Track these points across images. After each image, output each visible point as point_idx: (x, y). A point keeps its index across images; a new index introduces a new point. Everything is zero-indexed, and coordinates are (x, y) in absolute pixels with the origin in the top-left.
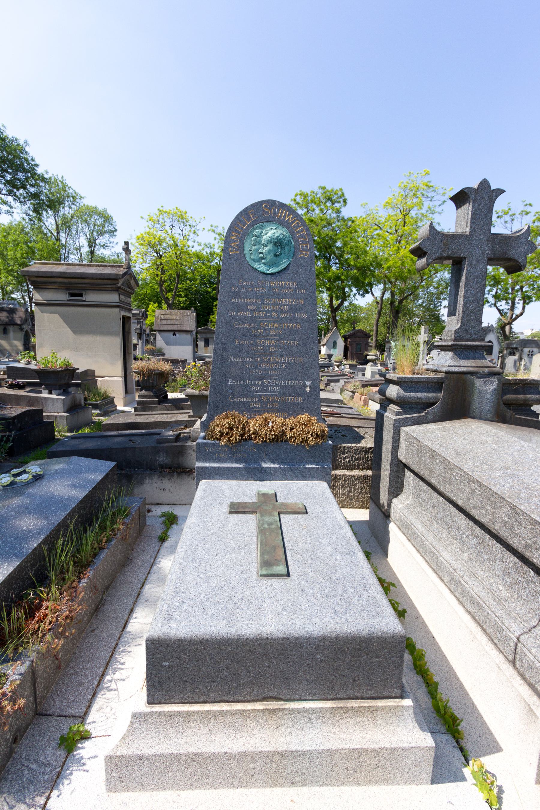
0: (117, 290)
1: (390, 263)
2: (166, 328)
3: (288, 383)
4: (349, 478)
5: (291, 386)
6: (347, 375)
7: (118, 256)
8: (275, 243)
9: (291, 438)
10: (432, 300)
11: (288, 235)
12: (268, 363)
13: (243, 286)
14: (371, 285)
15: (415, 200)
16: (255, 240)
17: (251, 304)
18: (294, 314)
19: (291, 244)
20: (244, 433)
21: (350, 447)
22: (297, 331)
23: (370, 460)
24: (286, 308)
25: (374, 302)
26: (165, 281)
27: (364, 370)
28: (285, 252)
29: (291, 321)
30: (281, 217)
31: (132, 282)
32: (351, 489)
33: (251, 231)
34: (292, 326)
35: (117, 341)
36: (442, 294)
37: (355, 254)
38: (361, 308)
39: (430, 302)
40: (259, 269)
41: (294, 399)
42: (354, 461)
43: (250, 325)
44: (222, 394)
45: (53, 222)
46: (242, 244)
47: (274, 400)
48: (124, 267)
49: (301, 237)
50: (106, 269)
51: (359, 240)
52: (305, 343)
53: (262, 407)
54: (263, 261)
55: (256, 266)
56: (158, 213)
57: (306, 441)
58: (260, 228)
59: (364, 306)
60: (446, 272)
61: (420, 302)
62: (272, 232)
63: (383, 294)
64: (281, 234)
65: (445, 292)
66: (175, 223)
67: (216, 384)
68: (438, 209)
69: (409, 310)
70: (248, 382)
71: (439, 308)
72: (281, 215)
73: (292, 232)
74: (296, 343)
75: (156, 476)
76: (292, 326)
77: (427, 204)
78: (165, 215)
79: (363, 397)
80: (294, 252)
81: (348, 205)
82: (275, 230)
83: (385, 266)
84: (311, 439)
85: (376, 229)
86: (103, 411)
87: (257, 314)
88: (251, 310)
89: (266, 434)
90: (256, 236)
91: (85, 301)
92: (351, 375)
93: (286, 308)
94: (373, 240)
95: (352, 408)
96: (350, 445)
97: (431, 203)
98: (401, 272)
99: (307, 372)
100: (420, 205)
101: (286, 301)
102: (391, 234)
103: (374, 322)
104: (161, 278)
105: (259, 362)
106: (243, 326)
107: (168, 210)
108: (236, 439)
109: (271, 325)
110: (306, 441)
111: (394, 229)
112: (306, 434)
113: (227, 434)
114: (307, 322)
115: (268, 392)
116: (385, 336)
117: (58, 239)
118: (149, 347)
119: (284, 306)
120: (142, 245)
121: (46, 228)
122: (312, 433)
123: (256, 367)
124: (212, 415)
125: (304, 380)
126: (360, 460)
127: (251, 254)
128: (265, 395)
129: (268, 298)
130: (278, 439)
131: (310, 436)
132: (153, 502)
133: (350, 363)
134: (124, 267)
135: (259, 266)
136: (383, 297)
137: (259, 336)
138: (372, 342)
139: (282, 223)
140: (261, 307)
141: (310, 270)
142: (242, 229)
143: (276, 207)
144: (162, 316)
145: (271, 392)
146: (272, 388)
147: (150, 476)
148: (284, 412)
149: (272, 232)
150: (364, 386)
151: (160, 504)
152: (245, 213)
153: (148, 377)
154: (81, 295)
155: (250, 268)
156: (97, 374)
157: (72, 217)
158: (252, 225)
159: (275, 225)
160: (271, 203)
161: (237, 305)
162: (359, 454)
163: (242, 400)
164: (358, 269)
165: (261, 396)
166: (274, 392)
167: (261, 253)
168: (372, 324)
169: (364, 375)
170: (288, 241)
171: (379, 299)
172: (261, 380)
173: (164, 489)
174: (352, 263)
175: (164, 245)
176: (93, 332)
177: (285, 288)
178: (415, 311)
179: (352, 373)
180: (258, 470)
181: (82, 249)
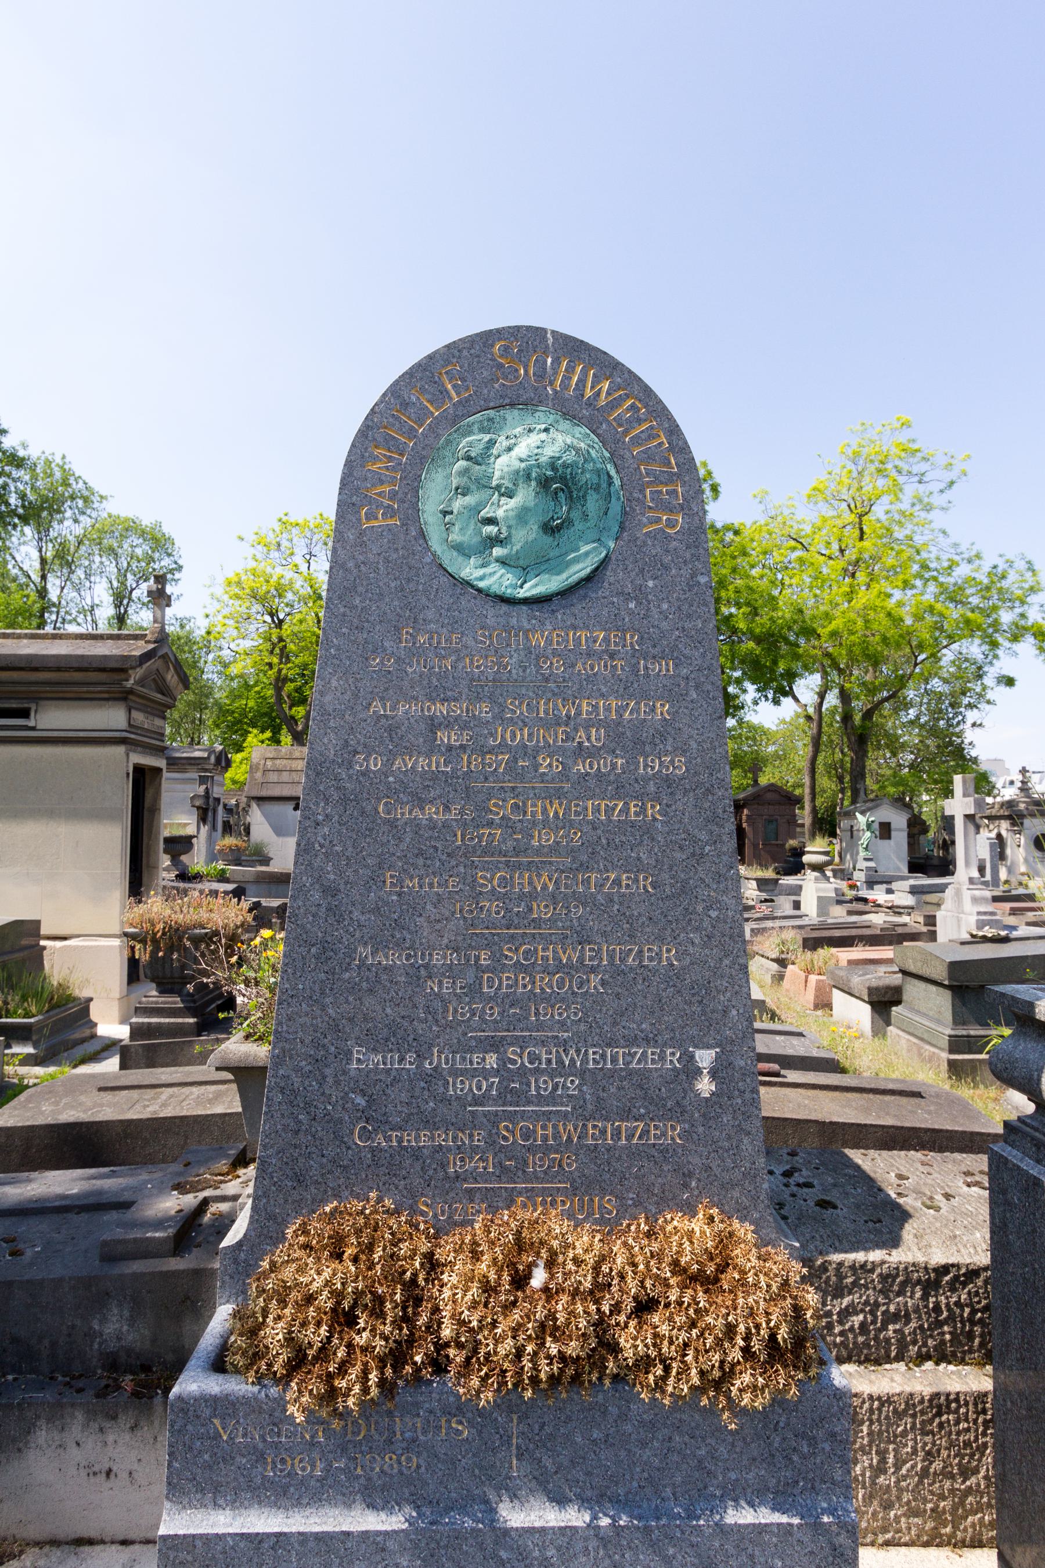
0: (125, 697)
1: (836, 624)
2: (276, 792)
3: (614, 1060)
4: (871, 1410)
5: (631, 1073)
6: (753, 907)
7: (182, 626)
8: (544, 483)
9: (644, 1363)
10: (941, 711)
11: (598, 452)
12: (525, 969)
13: (415, 652)
14: (791, 676)
15: (881, 482)
16: (466, 471)
17: (448, 723)
18: (632, 761)
19: (610, 483)
20: (411, 1341)
21: (863, 1266)
22: (647, 830)
23: (946, 1322)
24: (596, 737)
25: (798, 716)
26: (286, 680)
27: (797, 890)
28: (585, 516)
29: (620, 787)
30: (565, 386)
31: (171, 678)
32: (883, 1460)
33: (448, 442)
34: (626, 810)
35: (114, 837)
36: (964, 694)
37: (748, 604)
38: (765, 732)
39: (937, 713)
40: (481, 584)
41: (645, 1132)
42: (884, 1327)
43: (447, 809)
44: (320, 1113)
45: (35, 555)
46: (413, 487)
47: (556, 1136)
48: (148, 638)
49: (649, 457)
50: (100, 643)
51: (755, 572)
52: (685, 882)
53: (504, 1172)
54: (497, 551)
55: (470, 570)
56: (278, 527)
57: (717, 1385)
58: (483, 430)
59: (774, 728)
60: (977, 641)
61: (912, 712)
62: (530, 442)
63: (822, 696)
64: (569, 447)
65: (969, 690)
66: (318, 548)
67: (298, 1070)
68: (937, 500)
69: (887, 734)
70: (438, 1059)
71: (961, 727)
72: (567, 378)
73: (612, 443)
74: (645, 882)
75: (80, 1416)
76: (626, 810)
77: (911, 489)
78: (294, 531)
79: (813, 978)
80: (625, 513)
81: (721, 497)
82: (543, 436)
83: (824, 632)
84: (747, 1378)
85: (793, 549)
86: (43, 1046)
87: (476, 762)
88: (450, 748)
89: (519, 1353)
90: (468, 458)
91: (33, 729)
92: (764, 906)
93: (596, 737)
94: (790, 572)
95: (800, 1035)
96: (860, 1256)
97: (921, 487)
98: (865, 644)
99: (697, 1008)
100: (897, 489)
101: (596, 707)
102: (830, 558)
103: (804, 764)
104: (280, 671)
105: (487, 969)
106: (417, 812)
107: (301, 521)
108: (365, 1390)
109: (535, 809)
110: (717, 1385)
111: (835, 546)
112: (719, 1342)
113: (325, 1352)
114: (686, 792)
115: (529, 1103)
116: (835, 795)
117: (43, 593)
118: (230, 841)
119: (587, 728)
120: (238, 597)
121: (17, 564)
122: (747, 1338)
123: (473, 991)
124: (272, 1217)
125: (685, 1044)
126: (908, 1321)
127: (448, 527)
128: (511, 1117)
129: (520, 697)
130: (576, 1379)
131: (736, 1355)
132: (61, 1536)
133: (760, 874)
134: (148, 638)
135: (481, 572)
136: (821, 704)
137: (485, 853)
138: (805, 816)
139: (570, 409)
140: (493, 734)
141: (692, 584)
142: (411, 433)
143: (546, 353)
144: (269, 763)
145: (540, 1099)
146: (545, 1085)
147: (56, 1414)
148: (603, 1192)
149: (530, 442)
150: (812, 944)
151: (90, 1542)
152: (425, 374)
153: (171, 949)
154: (25, 714)
155: (445, 579)
156: (43, 931)
157: (80, 543)
158: (454, 421)
159: (543, 417)
160: (527, 340)
161: (390, 730)
162: (898, 1294)
163: (409, 1139)
164: (758, 640)
165: (494, 1119)
166: (552, 1099)
167: (491, 521)
168: (800, 771)
169: (797, 905)
170: (598, 472)
171: (811, 710)
172: (495, 1045)
173: (109, 1472)
174: (742, 625)
175: (290, 596)
176: (51, 813)
177: (590, 654)
178: (901, 736)
179: (766, 901)
180: (481, 1547)
181: (97, 612)
